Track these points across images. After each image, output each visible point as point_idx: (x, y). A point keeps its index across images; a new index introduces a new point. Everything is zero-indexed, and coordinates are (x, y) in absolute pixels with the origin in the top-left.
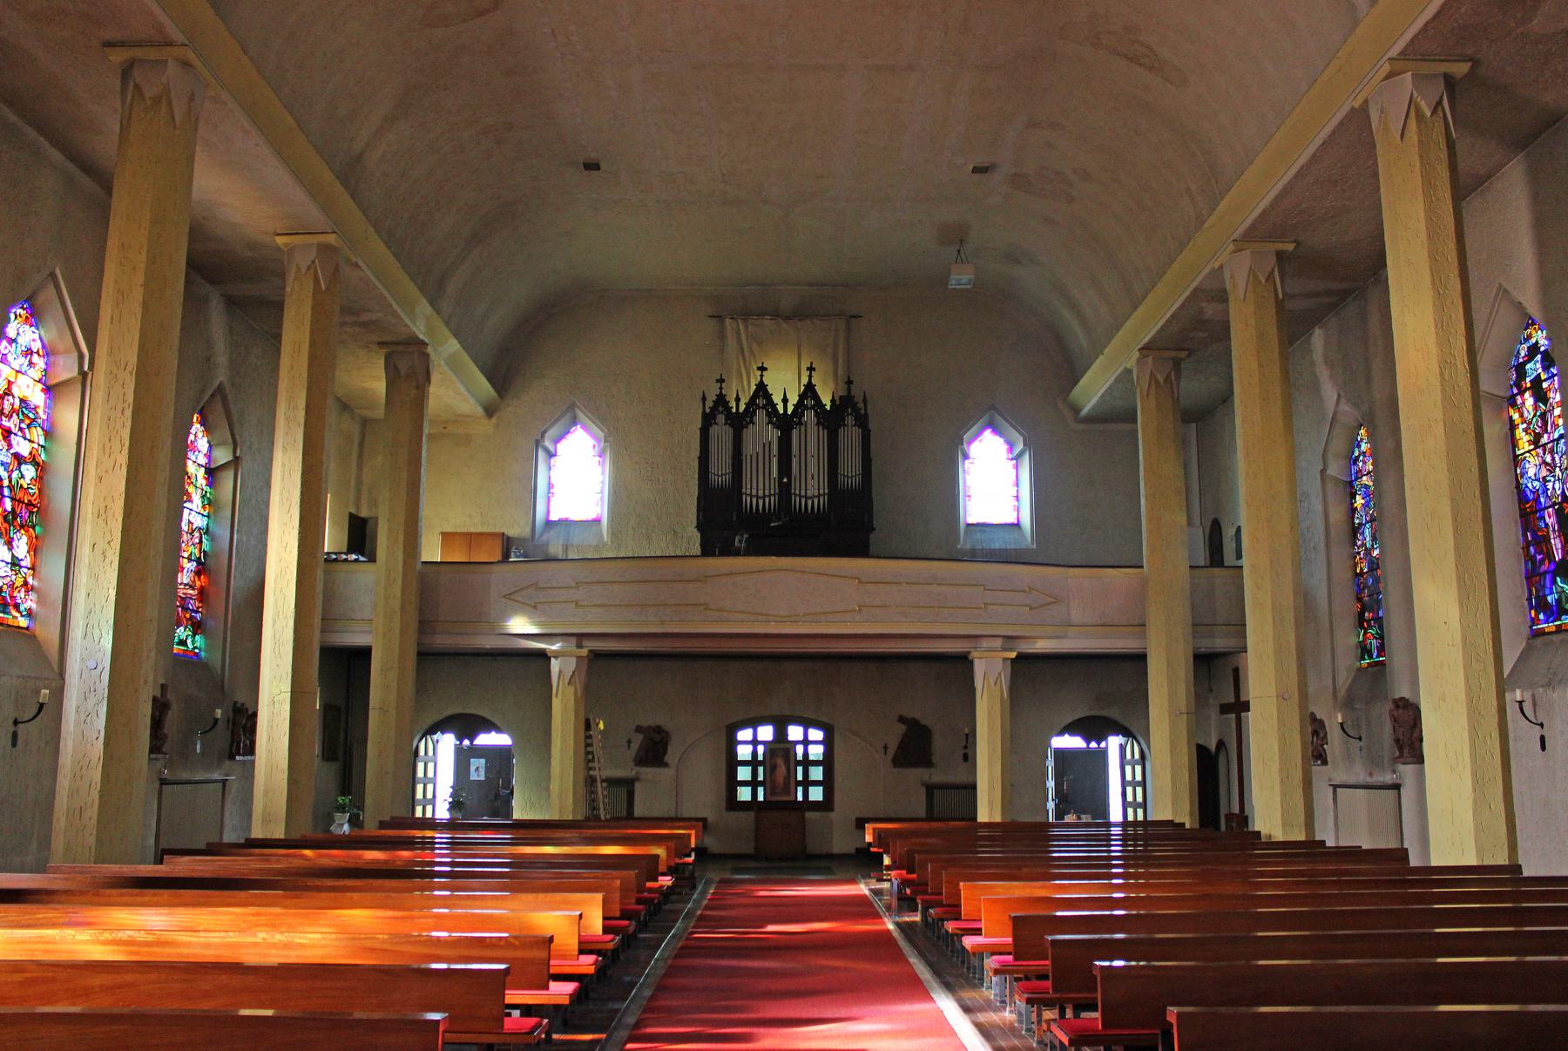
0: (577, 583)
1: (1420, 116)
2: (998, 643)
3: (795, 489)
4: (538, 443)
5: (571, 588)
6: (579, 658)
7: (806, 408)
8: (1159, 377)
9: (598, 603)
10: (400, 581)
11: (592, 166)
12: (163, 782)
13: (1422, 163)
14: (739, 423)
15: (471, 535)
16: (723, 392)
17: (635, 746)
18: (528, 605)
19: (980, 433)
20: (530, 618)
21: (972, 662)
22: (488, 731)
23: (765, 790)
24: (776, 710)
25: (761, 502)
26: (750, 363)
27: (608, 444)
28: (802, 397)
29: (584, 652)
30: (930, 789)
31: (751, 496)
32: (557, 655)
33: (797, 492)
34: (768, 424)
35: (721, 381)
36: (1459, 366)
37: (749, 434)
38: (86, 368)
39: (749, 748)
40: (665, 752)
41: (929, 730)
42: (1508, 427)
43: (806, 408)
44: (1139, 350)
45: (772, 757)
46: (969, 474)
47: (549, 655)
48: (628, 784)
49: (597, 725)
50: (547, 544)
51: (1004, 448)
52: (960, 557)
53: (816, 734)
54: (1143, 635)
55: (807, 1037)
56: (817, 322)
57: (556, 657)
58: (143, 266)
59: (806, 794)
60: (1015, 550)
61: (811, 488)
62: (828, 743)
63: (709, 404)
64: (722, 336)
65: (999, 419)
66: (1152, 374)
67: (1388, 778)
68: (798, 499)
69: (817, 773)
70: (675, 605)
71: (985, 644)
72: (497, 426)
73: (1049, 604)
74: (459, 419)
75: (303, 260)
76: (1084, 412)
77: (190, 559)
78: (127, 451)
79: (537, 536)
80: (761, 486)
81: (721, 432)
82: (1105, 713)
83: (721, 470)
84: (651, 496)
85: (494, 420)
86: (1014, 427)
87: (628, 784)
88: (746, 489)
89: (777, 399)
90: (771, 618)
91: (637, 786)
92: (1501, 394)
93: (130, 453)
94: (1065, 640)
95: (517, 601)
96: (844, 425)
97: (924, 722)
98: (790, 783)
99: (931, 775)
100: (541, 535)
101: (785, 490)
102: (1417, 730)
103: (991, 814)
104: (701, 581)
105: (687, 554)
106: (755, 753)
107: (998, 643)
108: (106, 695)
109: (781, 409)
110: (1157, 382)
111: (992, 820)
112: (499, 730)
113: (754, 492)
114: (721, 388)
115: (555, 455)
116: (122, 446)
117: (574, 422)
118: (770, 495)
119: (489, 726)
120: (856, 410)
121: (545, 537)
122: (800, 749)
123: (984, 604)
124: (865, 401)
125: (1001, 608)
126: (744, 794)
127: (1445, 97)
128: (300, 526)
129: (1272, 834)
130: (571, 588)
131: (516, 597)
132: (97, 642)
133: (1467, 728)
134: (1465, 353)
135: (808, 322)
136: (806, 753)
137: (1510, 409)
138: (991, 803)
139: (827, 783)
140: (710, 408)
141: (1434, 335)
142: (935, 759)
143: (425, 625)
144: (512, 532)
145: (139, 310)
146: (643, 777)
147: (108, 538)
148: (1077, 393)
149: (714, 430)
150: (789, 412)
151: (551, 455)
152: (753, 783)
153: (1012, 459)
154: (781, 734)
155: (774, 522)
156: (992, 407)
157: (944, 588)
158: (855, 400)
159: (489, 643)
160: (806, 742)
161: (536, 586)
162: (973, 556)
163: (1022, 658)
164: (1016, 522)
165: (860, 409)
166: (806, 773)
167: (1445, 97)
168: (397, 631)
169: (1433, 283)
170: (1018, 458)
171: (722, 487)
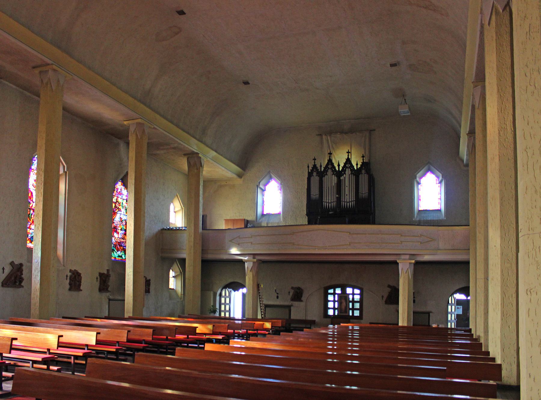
1: (497, 13)
2: (408, 257)
3: (343, 199)
4: (258, 186)
5: (249, 237)
6: (254, 262)
7: (347, 167)
10: (193, 236)
12: (110, 300)
13: (496, 35)
14: (322, 175)
15: (234, 220)
16: (316, 164)
17: (291, 294)
20: (237, 248)
21: (398, 264)
23: (338, 311)
24: (341, 282)
25: (348, 204)
28: (345, 164)
29: (255, 260)
31: (326, 202)
32: (247, 261)
33: (343, 200)
34: (333, 175)
35: (315, 159)
36: (508, 129)
37: (325, 179)
38: (66, 170)
40: (302, 296)
43: (347, 167)
46: (420, 190)
47: (244, 261)
48: (289, 307)
49: (261, 286)
50: (261, 222)
52: (414, 224)
53: (357, 291)
54: (468, 254)
56: (358, 134)
57: (246, 262)
58: (44, 138)
59: (353, 313)
60: (437, 220)
62: (361, 294)
63: (310, 168)
64: (322, 142)
65: (432, 168)
69: (357, 306)
70: (283, 243)
71: (403, 257)
72: (244, 181)
73: (429, 241)
74: (230, 179)
75: (132, 129)
77: (121, 230)
79: (258, 220)
81: (315, 179)
83: (315, 193)
85: (242, 179)
86: (438, 171)
87: (289, 307)
90: (317, 248)
91: (292, 308)
93: (43, 197)
94: (436, 256)
95: (234, 243)
96: (361, 174)
98: (347, 309)
100: (260, 219)
101: (339, 200)
103: (403, 322)
108: (40, 270)
109: (337, 169)
111: (404, 325)
114: (315, 162)
116: (41, 194)
117: (271, 178)
118: (333, 202)
122: (351, 297)
123: (401, 242)
126: (331, 312)
128: (134, 218)
129: (480, 335)
130: (249, 237)
131: (233, 241)
133: (500, 292)
134: (512, 123)
136: (353, 298)
138: (403, 318)
139: (361, 309)
140: (310, 170)
141: (497, 116)
144: (249, 218)
145: (44, 151)
146: (294, 305)
147: (39, 223)
149: (312, 178)
150: (340, 170)
155: (331, 212)
156: (429, 163)
158: (317, 166)
159: (225, 257)
160: (353, 294)
162: (419, 223)
163: (417, 263)
164: (439, 209)
166: (353, 305)
167: (494, 1)
168: (193, 253)
169: (498, 91)
170: (440, 183)
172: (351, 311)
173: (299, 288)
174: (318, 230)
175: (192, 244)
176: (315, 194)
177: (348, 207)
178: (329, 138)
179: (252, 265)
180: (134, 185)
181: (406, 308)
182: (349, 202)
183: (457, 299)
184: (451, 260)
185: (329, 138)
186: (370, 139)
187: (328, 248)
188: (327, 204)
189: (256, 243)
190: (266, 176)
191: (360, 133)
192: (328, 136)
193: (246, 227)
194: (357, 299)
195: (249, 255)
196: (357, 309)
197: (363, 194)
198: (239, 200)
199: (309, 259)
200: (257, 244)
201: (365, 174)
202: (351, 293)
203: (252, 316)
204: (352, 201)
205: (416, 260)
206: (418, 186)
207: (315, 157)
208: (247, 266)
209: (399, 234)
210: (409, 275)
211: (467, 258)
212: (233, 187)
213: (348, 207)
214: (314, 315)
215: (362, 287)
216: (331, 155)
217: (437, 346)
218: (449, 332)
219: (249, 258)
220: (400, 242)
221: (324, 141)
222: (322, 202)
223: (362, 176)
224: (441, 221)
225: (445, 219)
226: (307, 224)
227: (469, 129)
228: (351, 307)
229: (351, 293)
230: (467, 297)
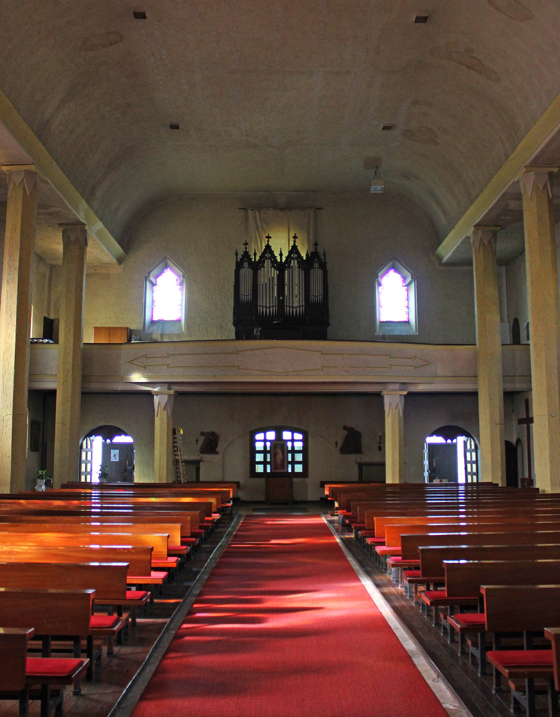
2: (397, 386)
4: (146, 278)
6: (169, 395)
11: (174, 127)
14: (256, 267)
15: (110, 328)
17: (200, 443)
19: (387, 272)
27: (185, 279)
28: (290, 252)
29: (172, 392)
31: (262, 306)
32: (157, 394)
34: (272, 267)
35: (246, 244)
39: (262, 444)
40: (216, 446)
43: (266, 258)
48: (196, 464)
50: (151, 334)
53: (298, 436)
54: (476, 382)
57: (157, 395)
59: (293, 468)
62: (305, 441)
63: (240, 257)
64: (246, 219)
65: (398, 264)
66: (481, 239)
68: (261, 308)
69: (299, 457)
71: (391, 387)
72: (124, 269)
76: (445, 260)
81: (246, 272)
83: (246, 292)
85: (122, 266)
86: (404, 267)
87: (196, 464)
89: (277, 254)
90: (273, 373)
91: (202, 464)
96: (313, 268)
97: (357, 429)
100: (149, 328)
101: (281, 304)
103: (393, 479)
106: (265, 446)
109: (278, 259)
111: (394, 482)
112: (126, 434)
114: (246, 248)
115: (156, 285)
117: (166, 266)
121: (150, 330)
122: (289, 444)
124: (324, 254)
126: (260, 469)
131: (135, 362)
136: (293, 447)
139: (305, 462)
140: (240, 259)
142: (363, 449)
143: (85, 378)
144: (133, 327)
146: (204, 459)
149: (242, 271)
150: (283, 261)
152: (265, 463)
153: (405, 286)
154: (279, 436)
155: (275, 321)
158: (320, 254)
159: (120, 387)
160: (293, 440)
161: (146, 356)
162: (384, 339)
163: (410, 394)
164: (407, 320)
165: (322, 259)
166: (293, 457)
170: (408, 285)
172: (290, 466)
173: (213, 434)
174: (276, 347)
175: (70, 366)
177: (264, 315)
178: (257, 215)
179: (167, 399)
180: (18, 270)
181: (397, 457)
183: (428, 443)
184: (447, 390)
185: (257, 215)
187: (290, 374)
188: (264, 309)
190: (159, 263)
192: (256, 211)
193: (129, 340)
194: (299, 447)
195: (161, 384)
196: (299, 463)
198: (116, 298)
202: (290, 438)
203: (167, 479)
204: (273, 307)
205: (409, 390)
206: (378, 288)
207: (246, 241)
208: (158, 402)
209: (320, 352)
210: (399, 410)
211: (473, 388)
212: (107, 276)
213: (264, 315)
215: (306, 429)
217: (501, 507)
219: (162, 388)
220: (389, 367)
222: (257, 306)
223: (314, 271)
224: (412, 336)
225: (417, 333)
226: (234, 337)
227: (480, 221)
229: (290, 438)
230: (446, 441)
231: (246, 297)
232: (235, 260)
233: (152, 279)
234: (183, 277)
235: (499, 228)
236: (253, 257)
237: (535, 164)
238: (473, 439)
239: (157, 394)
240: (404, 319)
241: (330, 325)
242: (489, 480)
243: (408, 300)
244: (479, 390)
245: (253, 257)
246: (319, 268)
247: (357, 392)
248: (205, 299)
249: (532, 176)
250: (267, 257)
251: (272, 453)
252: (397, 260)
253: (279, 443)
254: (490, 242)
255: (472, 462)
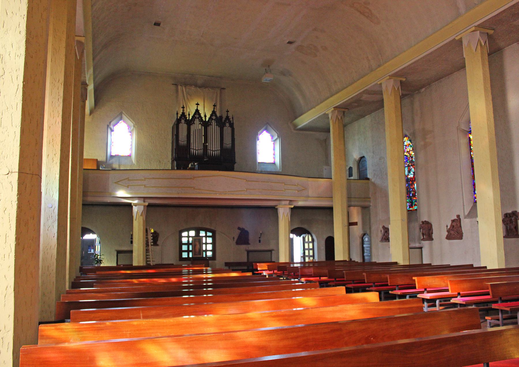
0: (145, 178)
2: (288, 202)
4: (108, 126)
6: (144, 206)
8: (339, 117)
9: (153, 186)
11: (157, 24)
14: (190, 123)
18: (125, 186)
19: (262, 132)
22: (89, 233)
24: (196, 225)
25: (197, 152)
26: (187, 103)
27: (135, 128)
28: (211, 115)
29: (147, 204)
30: (248, 252)
31: (194, 149)
32: (136, 205)
33: (210, 149)
37: (193, 128)
39: (186, 239)
41: (248, 232)
42: (469, 140)
43: (196, 118)
44: (334, 108)
45: (194, 242)
46: (259, 145)
50: (112, 163)
51: (270, 137)
55: (112, 341)
61: (214, 148)
63: (179, 115)
65: (269, 128)
66: (337, 116)
67: (417, 245)
68: (210, 151)
71: (283, 203)
73: (303, 190)
76: (299, 127)
78: (61, 116)
79: (108, 161)
80: (197, 146)
81: (183, 126)
82: (303, 226)
84: (151, 148)
88: (192, 147)
89: (202, 115)
90: (217, 193)
92: (468, 130)
95: (121, 185)
97: (246, 229)
99: (248, 247)
101: (205, 147)
102: (431, 230)
104: (192, 179)
105: (164, 169)
106: (188, 241)
107: (288, 202)
110: (338, 119)
111: (286, 262)
112: (93, 233)
113: (195, 148)
115: (113, 131)
117: (121, 119)
118: (200, 149)
119: (90, 231)
120: (230, 122)
121: (111, 161)
123: (246, 189)
124: (233, 118)
125: (280, 191)
126: (185, 255)
127: (487, 40)
131: (120, 183)
132: (51, 196)
135: (207, 89)
137: (469, 135)
142: (250, 242)
143: (85, 194)
144: (99, 159)
148: (297, 121)
150: (207, 120)
151: (112, 131)
152: (188, 251)
153: (273, 141)
154: (197, 234)
155: (206, 159)
156: (267, 123)
157: (273, 184)
158: (230, 118)
161: (128, 179)
163: (296, 208)
165: (231, 121)
166: (188, 248)
167: (487, 40)
171: (183, 145)
176: (227, 144)
177: (210, 155)
182: (198, 150)
186: (221, 96)
188: (195, 151)
189: (151, 186)
191: (212, 89)
192: (183, 86)
196: (185, 251)
197: (227, 144)
199: (185, 203)
200: (152, 187)
201: (229, 127)
205: (295, 205)
210: (288, 217)
214: (170, 258)
216: (215, 107)
218: (291, 266)
219: (139, 201)
220: (284, 190)
221: (180, 91)
228: (191, 247)
231: (183, 142)
232: (176, 118)
233: (112, 127)
234: (134, 127)
235: (347, 110)
236: (188, 116)
237: (396, 75)
238: (312, 236)
239: (136, 205)
240: (272, 161)
241: (236, 163)
242: (342, 259)
243: (274, 149)
244: (333, 206)
245: (188, 116)
246: (229, 126)
247: (253, 205)
248: (149, 143)
249: (392, 82)
250: (196, 117)
251: (193, 244)
252: (269, 124)
253: (197, 239)
254: (341, 118)
255: (309, 249)
